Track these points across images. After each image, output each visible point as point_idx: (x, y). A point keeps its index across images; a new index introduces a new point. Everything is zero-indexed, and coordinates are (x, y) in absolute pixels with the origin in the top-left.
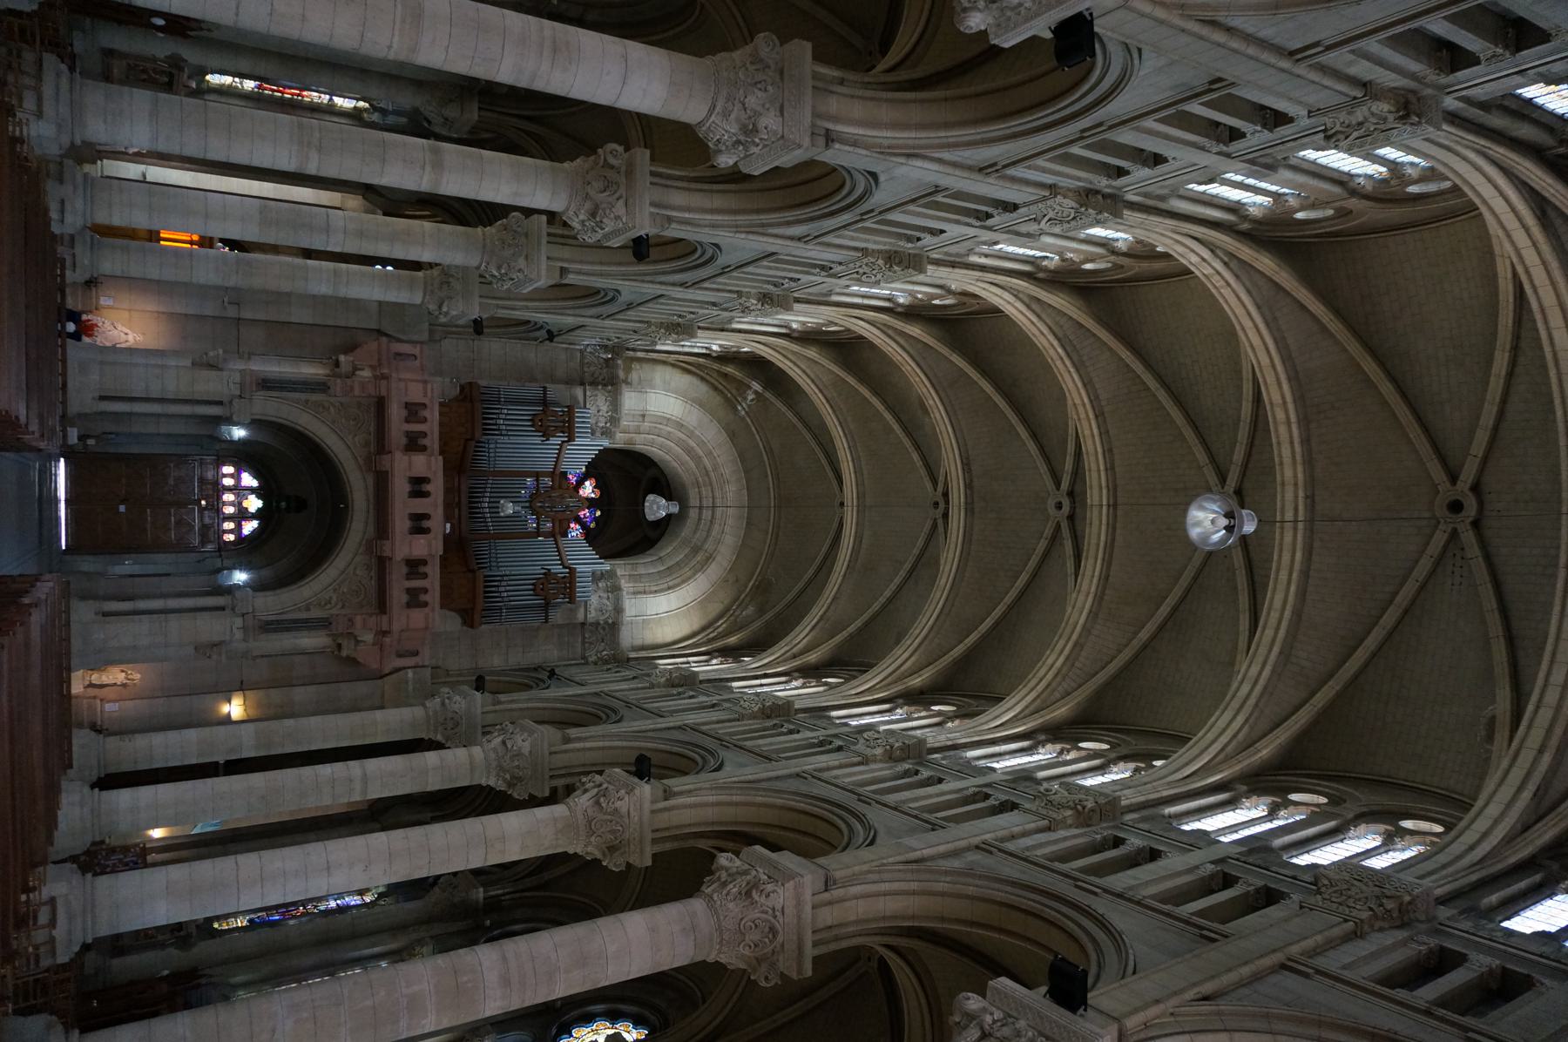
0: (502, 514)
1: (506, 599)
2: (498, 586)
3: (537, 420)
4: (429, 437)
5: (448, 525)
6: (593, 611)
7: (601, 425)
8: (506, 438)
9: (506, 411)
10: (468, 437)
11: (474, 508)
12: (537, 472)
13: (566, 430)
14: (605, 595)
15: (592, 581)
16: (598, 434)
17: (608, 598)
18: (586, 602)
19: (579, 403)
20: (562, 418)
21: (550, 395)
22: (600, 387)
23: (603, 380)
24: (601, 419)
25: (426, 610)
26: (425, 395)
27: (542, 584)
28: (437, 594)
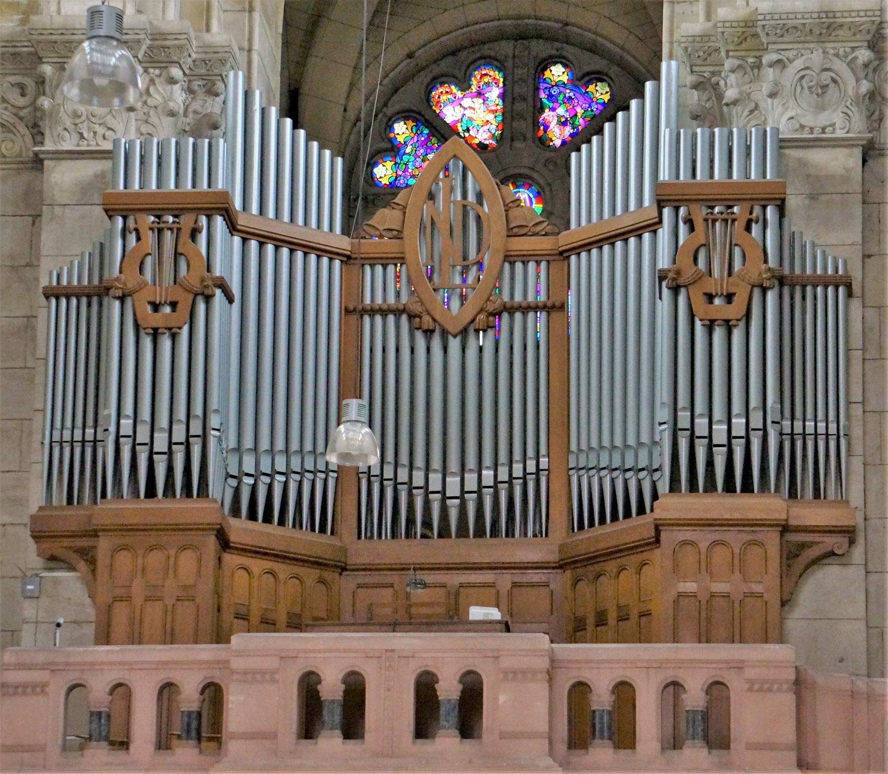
0: (374, 460)
1: (756, 421)
2: (710, 446)
3: (152, 319)
4: (175, 676)
5: (476, 613)
6: (823, 119)
7: (178, 96)
8: (214, 421)
9: (126, 425)
10: (212, 541)
11: (427, 523)
12: (347, 311)
13: (187, 221)
14: (770, 74)
15: (723, 121)
16: (213, 106)
17: (780, 64)
18: (783, 144)
19: (101, 176)
20: (150, 238)
21: (72, 278)
22: (45, 103)
23: (22, 89)
24: (156, 98)
25: (736, 684)
26: (40, 688)
27: (710, 298)
28: (689, 650)
